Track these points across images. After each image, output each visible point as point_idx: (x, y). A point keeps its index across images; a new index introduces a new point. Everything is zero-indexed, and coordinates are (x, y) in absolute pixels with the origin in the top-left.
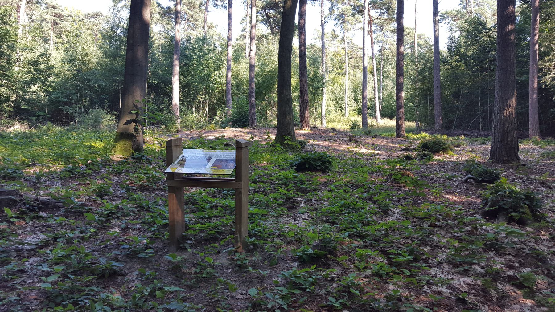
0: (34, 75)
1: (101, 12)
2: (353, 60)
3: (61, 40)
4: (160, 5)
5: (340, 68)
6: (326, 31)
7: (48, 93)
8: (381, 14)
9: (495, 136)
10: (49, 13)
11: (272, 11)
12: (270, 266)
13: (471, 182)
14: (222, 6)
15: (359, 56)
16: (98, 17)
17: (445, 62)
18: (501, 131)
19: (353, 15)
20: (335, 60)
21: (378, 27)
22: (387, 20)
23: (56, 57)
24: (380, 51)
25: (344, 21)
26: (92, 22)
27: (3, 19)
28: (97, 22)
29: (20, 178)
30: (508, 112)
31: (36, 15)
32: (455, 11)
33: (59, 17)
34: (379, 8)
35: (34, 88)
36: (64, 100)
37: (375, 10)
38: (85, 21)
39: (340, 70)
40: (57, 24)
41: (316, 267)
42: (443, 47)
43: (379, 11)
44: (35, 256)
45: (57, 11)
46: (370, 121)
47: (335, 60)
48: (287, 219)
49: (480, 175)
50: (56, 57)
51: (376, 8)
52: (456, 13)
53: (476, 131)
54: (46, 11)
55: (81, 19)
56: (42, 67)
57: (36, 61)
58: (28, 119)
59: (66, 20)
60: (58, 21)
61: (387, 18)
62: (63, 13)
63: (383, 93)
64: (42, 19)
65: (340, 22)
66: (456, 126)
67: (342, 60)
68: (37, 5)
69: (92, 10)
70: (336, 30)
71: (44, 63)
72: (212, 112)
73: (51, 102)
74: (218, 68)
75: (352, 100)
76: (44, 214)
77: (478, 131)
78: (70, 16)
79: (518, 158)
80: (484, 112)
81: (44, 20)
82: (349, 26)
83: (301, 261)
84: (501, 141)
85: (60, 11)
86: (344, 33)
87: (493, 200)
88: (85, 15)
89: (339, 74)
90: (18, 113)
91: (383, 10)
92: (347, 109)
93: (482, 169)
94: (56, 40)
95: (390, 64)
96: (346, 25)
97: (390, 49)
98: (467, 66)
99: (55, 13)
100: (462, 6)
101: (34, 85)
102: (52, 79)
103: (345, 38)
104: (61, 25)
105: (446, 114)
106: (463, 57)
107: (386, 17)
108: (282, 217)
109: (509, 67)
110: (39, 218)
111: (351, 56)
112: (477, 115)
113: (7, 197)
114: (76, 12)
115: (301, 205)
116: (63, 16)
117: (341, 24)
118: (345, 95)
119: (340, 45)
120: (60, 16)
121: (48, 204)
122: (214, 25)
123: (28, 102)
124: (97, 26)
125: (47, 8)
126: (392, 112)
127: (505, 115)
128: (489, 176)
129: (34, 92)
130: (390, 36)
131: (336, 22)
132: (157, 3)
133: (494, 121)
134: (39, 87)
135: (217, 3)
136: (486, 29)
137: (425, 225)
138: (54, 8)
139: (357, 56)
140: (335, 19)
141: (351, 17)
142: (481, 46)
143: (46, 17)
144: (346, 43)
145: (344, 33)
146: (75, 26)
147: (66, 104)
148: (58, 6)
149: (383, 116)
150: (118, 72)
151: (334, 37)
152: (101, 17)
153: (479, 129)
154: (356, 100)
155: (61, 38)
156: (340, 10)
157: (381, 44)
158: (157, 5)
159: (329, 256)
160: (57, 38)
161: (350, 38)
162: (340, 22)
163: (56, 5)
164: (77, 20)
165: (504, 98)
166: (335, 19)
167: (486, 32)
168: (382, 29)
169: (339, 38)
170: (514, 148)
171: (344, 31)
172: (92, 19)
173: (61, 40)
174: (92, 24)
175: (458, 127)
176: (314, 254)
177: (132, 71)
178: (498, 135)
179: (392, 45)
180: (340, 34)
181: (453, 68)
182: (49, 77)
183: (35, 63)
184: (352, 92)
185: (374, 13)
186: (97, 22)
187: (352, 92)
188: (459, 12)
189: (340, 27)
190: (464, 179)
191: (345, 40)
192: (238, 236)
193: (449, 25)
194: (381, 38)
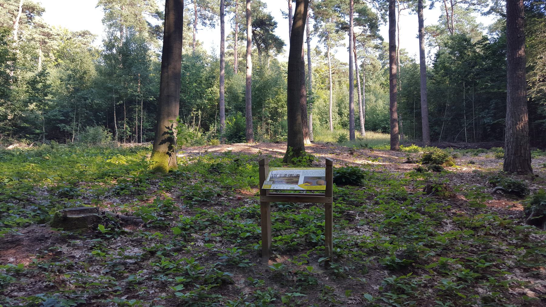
0: (31, 93)
1: (89, 30)
2: (335, 75)
3: (49, 59)
4: (149, 24)
5: (322, 83)
6: (311, 47)
7: (45, 112)
8: (365, 31)
9: (508, 150)
10: (38, 32)
11: (258, 29)
12: (362, 274)
13: (500, 193)
14: (210, 24)
15: (341, 71)
16: (86, 36)
17: (431, 77)
18: (514, 144)
19: (337, 31)
20: (318, 75)
21: (360, 43)
22: (370, 36)
23: (54, 75)
24: (361, 66)
25: (327, 38)
26: (80, 41)
27: (2, 40)
28: (85, 40)
29: (78, 196)
30: (520, 126)
31: (26, 34)
32: (434, 27)
33: (47, 36)
34: (362, 25)
35: (32, 106)
36: (61, 118)
37: (358, 27)
38: (72, 40)
39: (322, 85)
40: (46, 43)
41: (412, 275)
42: (430, 63)
43: (362, 27)
44: (141, 268)
45: (45, 30)
46: (357, 134)
47: (318, 75)
48: (350, 231)
49: (509, 186)
50: (54, 75)
51: (359, 25)
52: (435, 29)
53: (462, 143)
54: (34, 30)
55: (69, 37)
56: (39, 86)
57: (33, 81)
58: (26, 137)
59: (54, 39)
60: (47, 40)
61: (370, 34)
62: (51, 32)
63: (366, 106)
64: (31, 38)
65: (324, 38)
66: (442, 138)
67: (325, 75)
68: (27, 25)
69: (80, 29)
70: (319, 46)
71: (41, 82)
72: (205, 128)
73: (48, 121)
74: (210, 85)
75: (336, 114)
76: (126, 230)
77: (464, 143)
78: (58, 35)
79: (531, 170)
80: (469, 124)
81: (33, 39)
82: (333, 42)
83: (390, 270)
84: (515, 154)
85: (48, 30)
86: (328, 49)
87: (536, 210)
88: (74, 35)
89: (322, 89)
90: (19, 131)
91: (365, 26)
92: (332, 123)
93: (510, 180)
94: (44, 58)
95: (371, 79)
96: (329, 41)
97: (372, 64)
98: (452, 81)
99: (43, 32)
100: (441, 22)
101: (31, 103)
102: (49, 97)
103: (329, 54)
104: (50, 44)
105: (432, 126)
106: (447, 71)
107: (368, 33)
108: (344, 229)
109: (520, 84)
110: (123, 233)
111: (333, 71)
112: (462, 127)
113: (91, 214)
114: (63, 31)
115: (357, 218)
116: (51, 35)
117: (325, 40)
118: (329, 109)
119: (323, 61)
120: (48, 35)
121: (127, 220)
122: (200, 42)
123: (25, 120)
124: (85, 44)
125: (35, 27)
126: (375, 126)
127: (518, 128)
128: (517, 187)
129: (32, 111)
130: (372, 52)
131: (319, 39)
132: (147, 22)
133: (507, 135)
134: (36, 105)
135: (205, 21)
136: (471, 45)
137: (481, 233)
138: (43, 27)
139: (339, 71)
140: (319, 36)
141: (334, 34)
142: (466, 61)
143: (35, 36)
144: (330, 59)
145: (328, 49)
146: (63, 45)
147: (62, 121)
148: (47, 26)
149: (367, 129)
150: (112, 90)
151: (318, 53)
152: (89, 36)
153: (464, 141)
154: (340, 114)
155: (48, 56)
156: (323, 27)
157: (363, 60)
158: (146, 24)
159: (414, 264)
160: (45, 56)
161: (333, 54)
162: (324, 38)
163: (44, 25)
164: (65, 39)
165: (516, 114)
166: (319, 36)
167: (470, 48)
168: (363, 45)
169: (323, 54)
170: (527, 160)
171: (329, 47)
172: (80, 38)
173: (49, 59)
174: (80, 43)
175: (445, 139)
176: (402, 263)
177: (139, 91)
178: (512, 148)
179: (373, 60)
180: (323, 50)
181: (439, 83)
182: (46, 96)
183: (33, 83)
184: (336, 106)
185: (357, 30)
186: (85, 40)
187: (336, 106)
188: (438, 28)
189: (323, 44)
190: (494, 189)
191: (329, 56)
192: (329, 247)
193: (428, 40)
194: (363, 53)
